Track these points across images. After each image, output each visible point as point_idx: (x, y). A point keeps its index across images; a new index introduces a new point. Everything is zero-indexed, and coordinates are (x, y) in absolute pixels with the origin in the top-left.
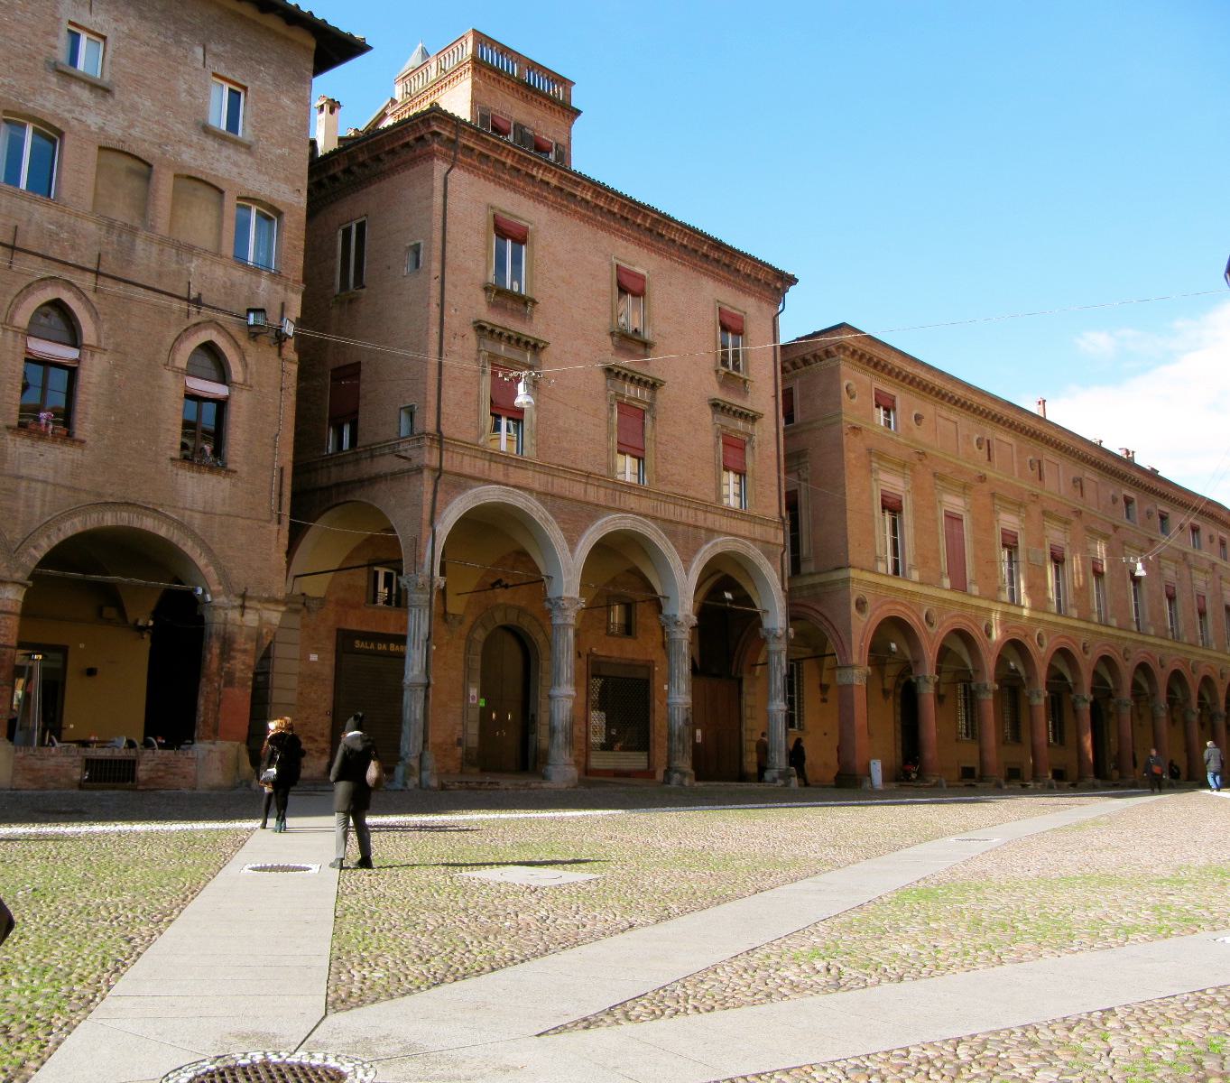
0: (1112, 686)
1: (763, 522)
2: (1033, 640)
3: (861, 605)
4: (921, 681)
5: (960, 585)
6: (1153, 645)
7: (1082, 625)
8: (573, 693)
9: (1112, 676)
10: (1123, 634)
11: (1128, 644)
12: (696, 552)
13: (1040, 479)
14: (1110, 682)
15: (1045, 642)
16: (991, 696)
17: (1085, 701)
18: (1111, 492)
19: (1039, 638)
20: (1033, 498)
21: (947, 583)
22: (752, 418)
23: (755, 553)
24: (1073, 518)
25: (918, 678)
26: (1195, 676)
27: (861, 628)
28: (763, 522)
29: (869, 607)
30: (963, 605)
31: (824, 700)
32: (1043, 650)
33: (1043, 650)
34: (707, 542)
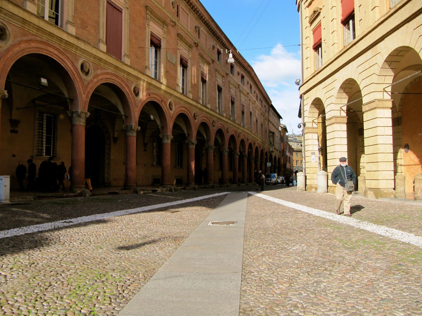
0: (206, 139)
2: (166, 106)
4: (74, 115)
5: (114, 48)
6: (225, 122)
11: (215, 119)
13: (178, 16)
14: (205, 136)
15: (173, 107)
16: (135, 134)
17: (193, 144)
18: (212, 44)
19: (170, 104)
20: (173, 24)
21: (103, 47)
25: (72, 113)
30: (117, 68)
31: (145, 150)
32: (172, 112)
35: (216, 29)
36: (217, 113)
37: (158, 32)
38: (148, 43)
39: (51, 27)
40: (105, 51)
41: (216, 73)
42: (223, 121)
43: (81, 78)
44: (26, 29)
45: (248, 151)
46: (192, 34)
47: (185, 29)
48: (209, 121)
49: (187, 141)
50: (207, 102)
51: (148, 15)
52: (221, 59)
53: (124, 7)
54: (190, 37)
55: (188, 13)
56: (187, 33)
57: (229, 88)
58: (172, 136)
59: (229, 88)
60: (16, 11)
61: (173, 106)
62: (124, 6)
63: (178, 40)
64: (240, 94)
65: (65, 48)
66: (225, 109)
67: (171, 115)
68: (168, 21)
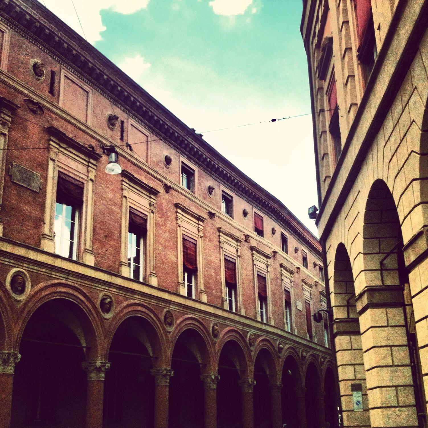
0: (151, 355)
9: (152, 346)
10: (166, 296)
14: (150, 350)
15: (29, 290)
26: (252, 348)
33: (22, 298)
35: (43, 21)
36: (258, 322)
37: (231, 253)
38: (125, 224)
39: (154, 289)
40: (186, 295)
41: (177, 212)
42: (200, 311)
43: (212, 340)
44: (53, 276)
45: (285, 373)
46: (100, 132)
47: (80, 122)
48: (156, 316)
49: (84, 364)
50: (148, 273)
51: (178, 214)
52: (194, 185)
53: (198, 238)
54: (93, 137)
55: (87, 88)
56: (83, 128)
57: (219, 242)
58: (19, 356)
59: (219, 242)
60: (32, 255)
61: (28, 285)
62: (197, 236)
63: (122, 181)
64: (252, 254)
65: (82, 284)
66: (206, 286)
67: (19, 306)
68: (19, 100)
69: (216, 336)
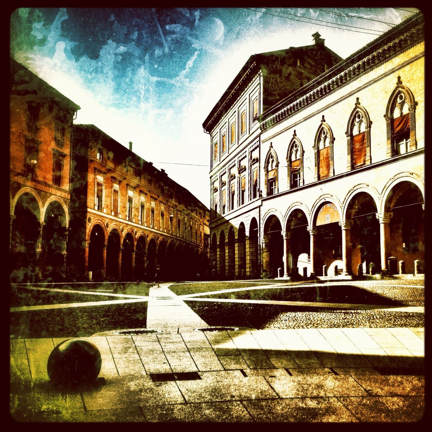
1: (65, 191)
3: (90, 220)
5: (116, 215)
7: (147, 228)
8: (199, 11)
12: (46, 200)
22: (64, 156)
23: (62, 201)
24: (148, 193)
27: (89, 227)
28: (65, 191)
29: (92, 221)
34: (49, 198)
69: (107, 227)
